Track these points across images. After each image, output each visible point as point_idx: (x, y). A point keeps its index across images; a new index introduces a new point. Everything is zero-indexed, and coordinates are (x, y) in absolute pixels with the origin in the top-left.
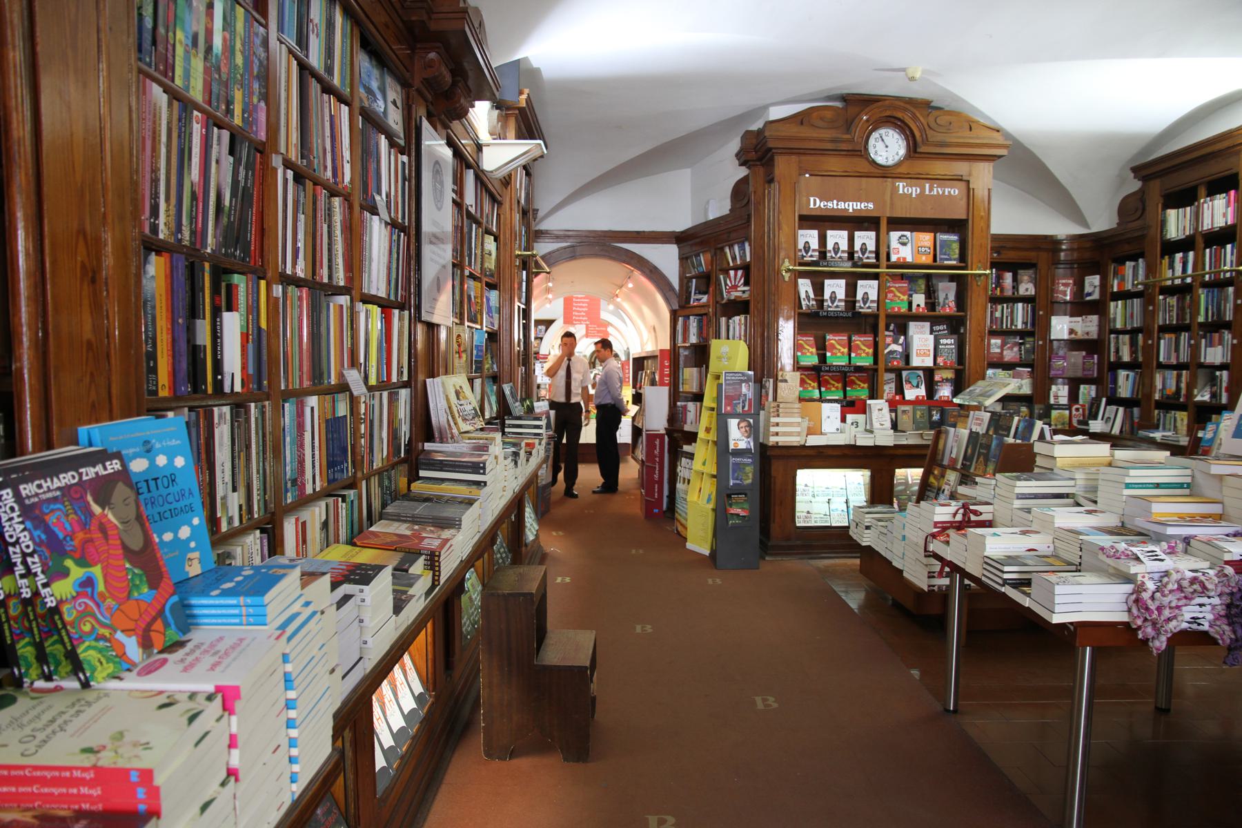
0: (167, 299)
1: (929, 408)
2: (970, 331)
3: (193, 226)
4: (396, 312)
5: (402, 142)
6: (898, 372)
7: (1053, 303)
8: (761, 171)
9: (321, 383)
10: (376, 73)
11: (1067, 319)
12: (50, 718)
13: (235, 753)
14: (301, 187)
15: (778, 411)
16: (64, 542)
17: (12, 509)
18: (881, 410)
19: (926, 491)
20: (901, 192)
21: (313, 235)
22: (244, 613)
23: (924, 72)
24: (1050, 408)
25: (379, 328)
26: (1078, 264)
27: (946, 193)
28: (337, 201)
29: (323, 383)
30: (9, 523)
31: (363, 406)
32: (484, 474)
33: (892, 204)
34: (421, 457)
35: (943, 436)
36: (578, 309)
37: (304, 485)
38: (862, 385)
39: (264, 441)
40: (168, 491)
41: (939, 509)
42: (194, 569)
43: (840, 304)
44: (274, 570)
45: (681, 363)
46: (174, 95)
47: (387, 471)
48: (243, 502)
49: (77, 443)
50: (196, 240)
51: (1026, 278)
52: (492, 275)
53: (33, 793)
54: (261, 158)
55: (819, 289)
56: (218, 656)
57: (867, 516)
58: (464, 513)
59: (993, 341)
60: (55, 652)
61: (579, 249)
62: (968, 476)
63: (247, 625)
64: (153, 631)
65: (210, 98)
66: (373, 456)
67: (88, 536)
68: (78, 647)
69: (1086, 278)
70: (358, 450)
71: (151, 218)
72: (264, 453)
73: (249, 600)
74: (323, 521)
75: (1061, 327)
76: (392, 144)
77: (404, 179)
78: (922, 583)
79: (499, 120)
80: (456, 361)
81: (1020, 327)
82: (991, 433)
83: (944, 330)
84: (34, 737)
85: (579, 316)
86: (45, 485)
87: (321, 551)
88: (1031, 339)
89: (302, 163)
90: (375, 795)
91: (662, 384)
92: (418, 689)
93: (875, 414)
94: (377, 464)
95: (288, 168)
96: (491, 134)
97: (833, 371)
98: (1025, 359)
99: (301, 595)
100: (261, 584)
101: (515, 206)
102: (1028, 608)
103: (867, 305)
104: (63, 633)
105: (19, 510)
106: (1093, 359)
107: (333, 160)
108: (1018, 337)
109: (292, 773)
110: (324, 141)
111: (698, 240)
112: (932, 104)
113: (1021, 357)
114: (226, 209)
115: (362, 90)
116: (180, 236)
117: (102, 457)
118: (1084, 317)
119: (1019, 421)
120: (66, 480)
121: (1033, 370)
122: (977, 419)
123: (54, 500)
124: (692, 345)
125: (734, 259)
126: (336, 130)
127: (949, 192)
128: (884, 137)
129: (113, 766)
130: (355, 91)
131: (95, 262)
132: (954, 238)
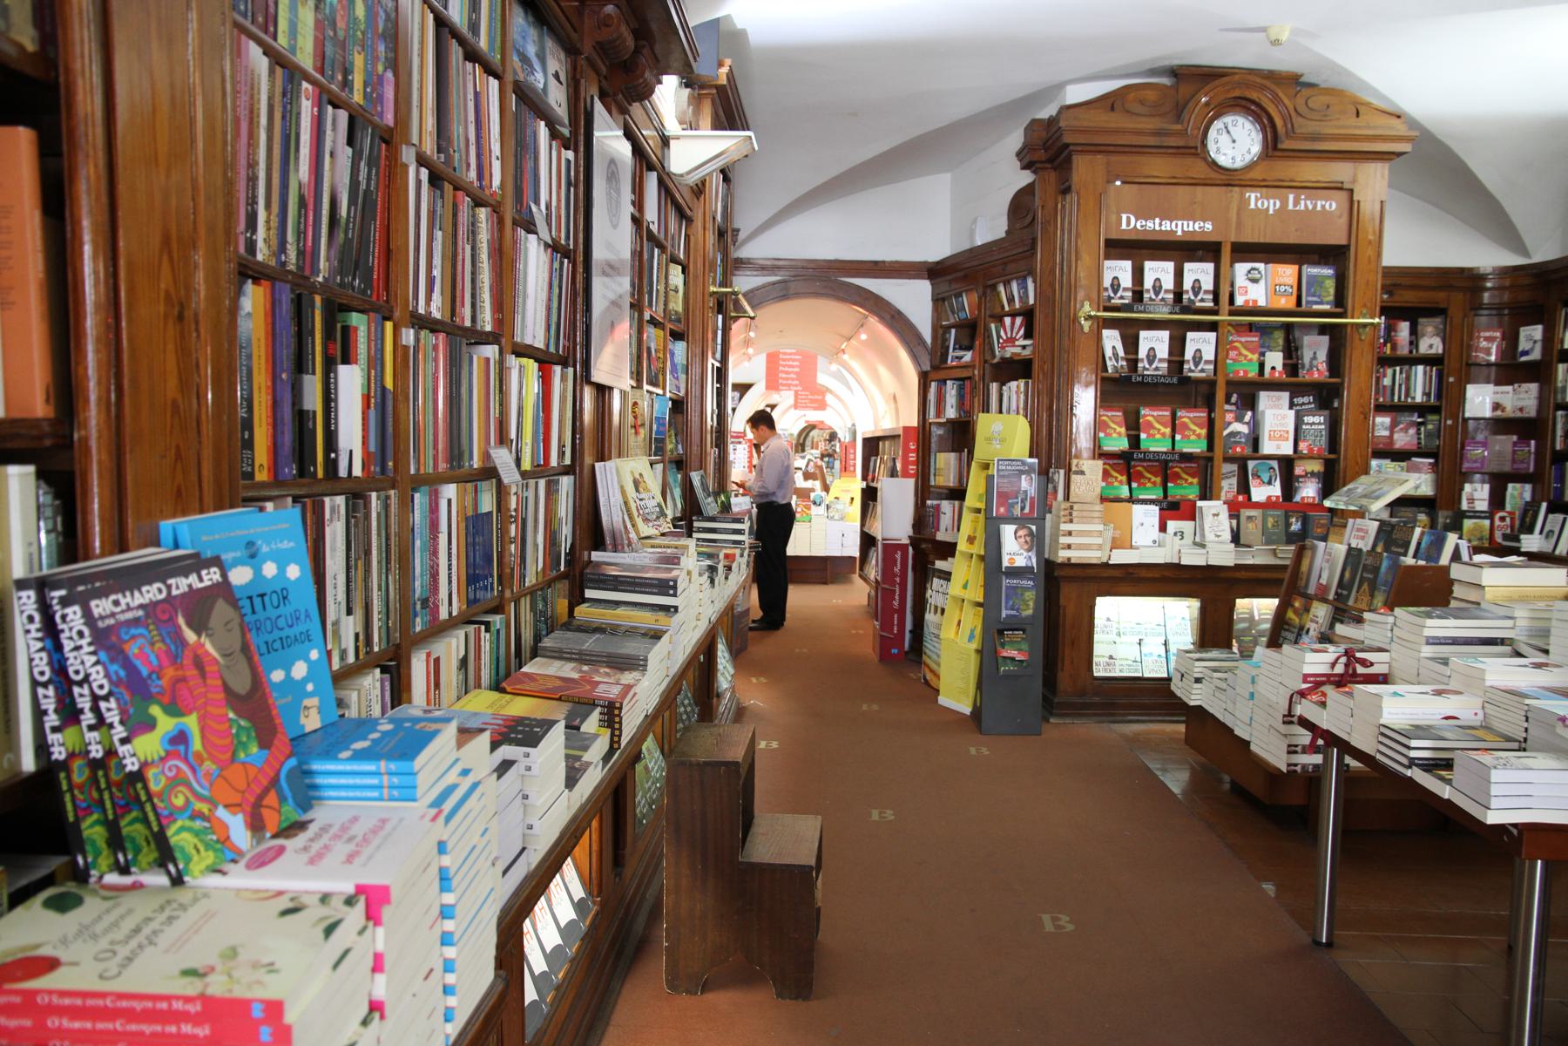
0: (267, 346)
1: (1286, 513)
2: (1348, 405)
3: (301, 245)
4: (557, 369)
5: (566, 132)
6: (1242, 463)
7: (1468, 365)
8: (1052, 176)
9: (460, 467)
10: (533, 33)
11: (1490, 388)
12: (133, 926)
13: (380, 979)
14: (438, 192)
15: (1071, 514)
16: (149, 682)
17: (81, 634)
18: (1217, 515)
19: (1281, 632)
20: (1252, 206)
21: (452, 259)
22: (386, 783)
23: (1295, 32)
24: (1462, 515)
25: (536, 391)
26: (1509, 308)
27: (1319, 208)
28: (483, 213)
29: (463, 467)
30: (75, 653)
31: (513, 499)
32: (675, 595)
33: (1239, 224)
34: (588, 571)
35: (1308, 553)
36: (786, 369)
37: (438, 607)
38: (1190, 480)
39: (388, 545)
40: (278, 612)
41: (1310, 657)
42: (312, 722)
43: (1161, 365)
44: (423, 724)
45: (933, 446)
46: (278, 60)
47: (542, 589)
48: (360, 629)
49: (158, 544)
50: (304, 263)
51: (1430, 329)
52: (679, 321)
53: (115, 1031)
54: (387, 150)
55: (1131, 344)
56: (354, 843)
57: (1197, 664)
58: (651, 649)
59: (1379, 420)
60: (134, 834)
61: (792, 285)
62: (1344, 611)
63: (390, 800)
64: (267, 807)
65: (323, 64)
66: (525, 568)
67: (180, 673)
68: (168, 827)
69: (1522, 329)
70: (506, 560)
71: (247, 232)
72: (388, 562)
73: (393, 766)
74: (461, 657)
75: (1480, 400)
76: (554, 135)
77: (569, 184)
78: (1278, 759)
79: (690, 104)
80: (632, 438)
81: (1419, 398)
82: (1379, 549)
83: (1309, 403)
84: (115, 953)
85: (787, 379)
86: (123, 601)
87: (459, 698)
88: (1435, 417)
89: (438, 158)
90: (523, 1040)
91: (906, 474)
92: (579, 892)
93: (1208, 521)
94: (530, 580)
95: (422, 165)
96: (681, 123)
97: (1150, 460)
98: (1426, 446)
99: (457, 760)
100: (409, 744)
101: (710, 225)
102: (1449, 800)
103: (1199, 368)
104: (148, 807)
105: (91, 636)
106: (1529, 446)
107: (479, 156)
108: (1416, 415)
109: (447, 1008)
110: (466, 128)
111: (960, 274)
112: (1302, 80)
113: (1419, 443)
114: (343, 221)
115: (515, 58)
116: (283, 258)
117: (196, 563)
118: (1516, 385)
119: (1422, 534)
120: (151, 595)
121: (1437, 461)
122: (1359, 530)
123: (136, 622)
124: (950, 421)
125: (1011, 300)
126: (482, 113)
127: (1323, 206)
128: (1230, 128)
129: (227, 995)
130: (508, 58)
131: (182, 292)
132: (1328, 272)
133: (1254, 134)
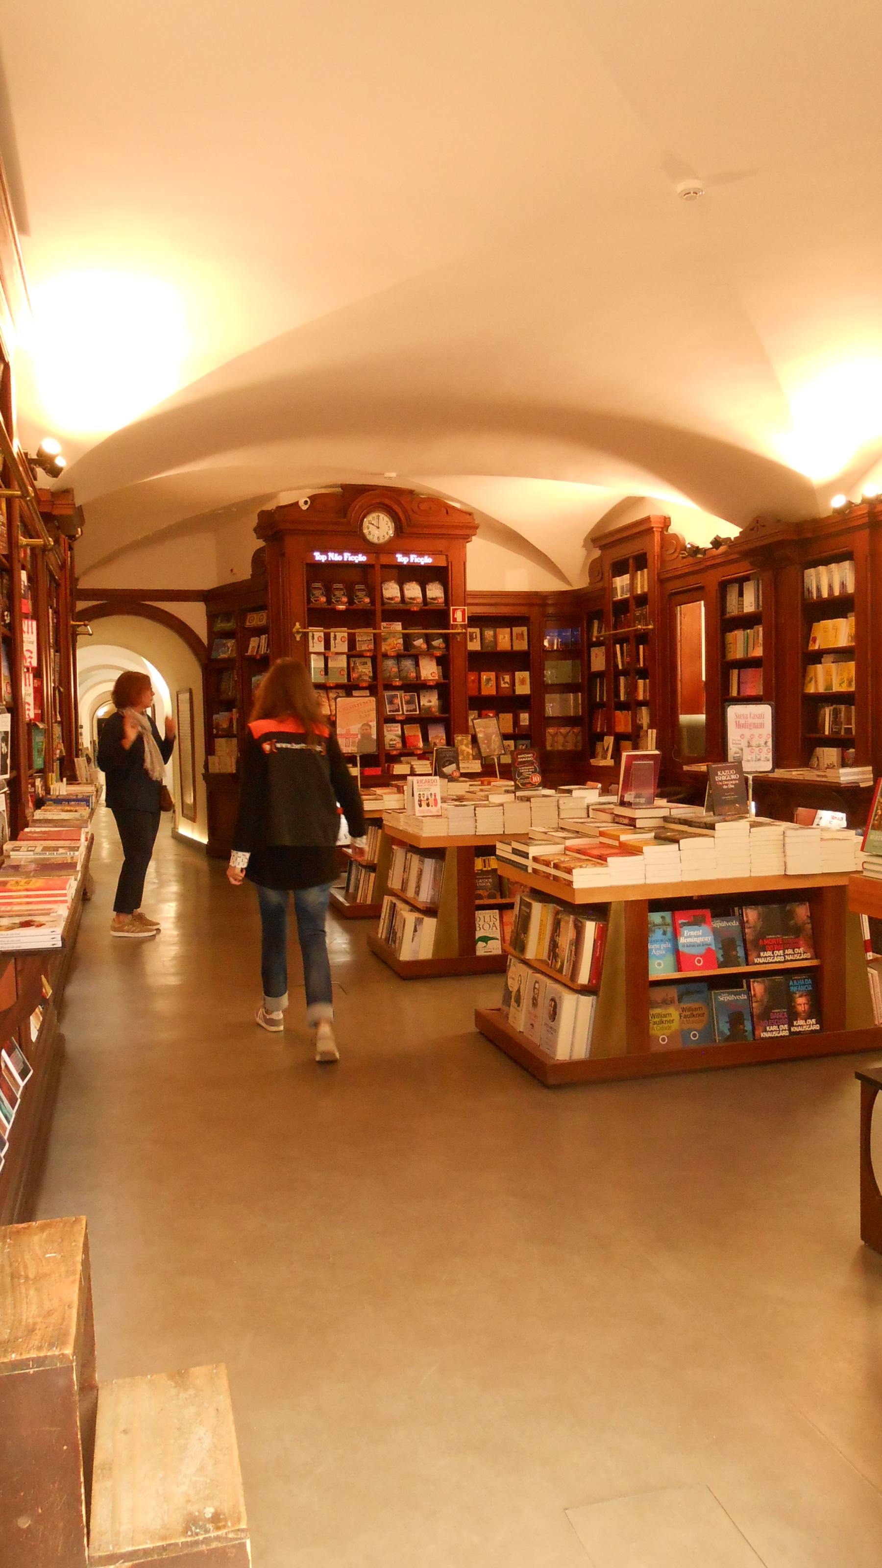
118: (65, 862)
133: (389, 523)
